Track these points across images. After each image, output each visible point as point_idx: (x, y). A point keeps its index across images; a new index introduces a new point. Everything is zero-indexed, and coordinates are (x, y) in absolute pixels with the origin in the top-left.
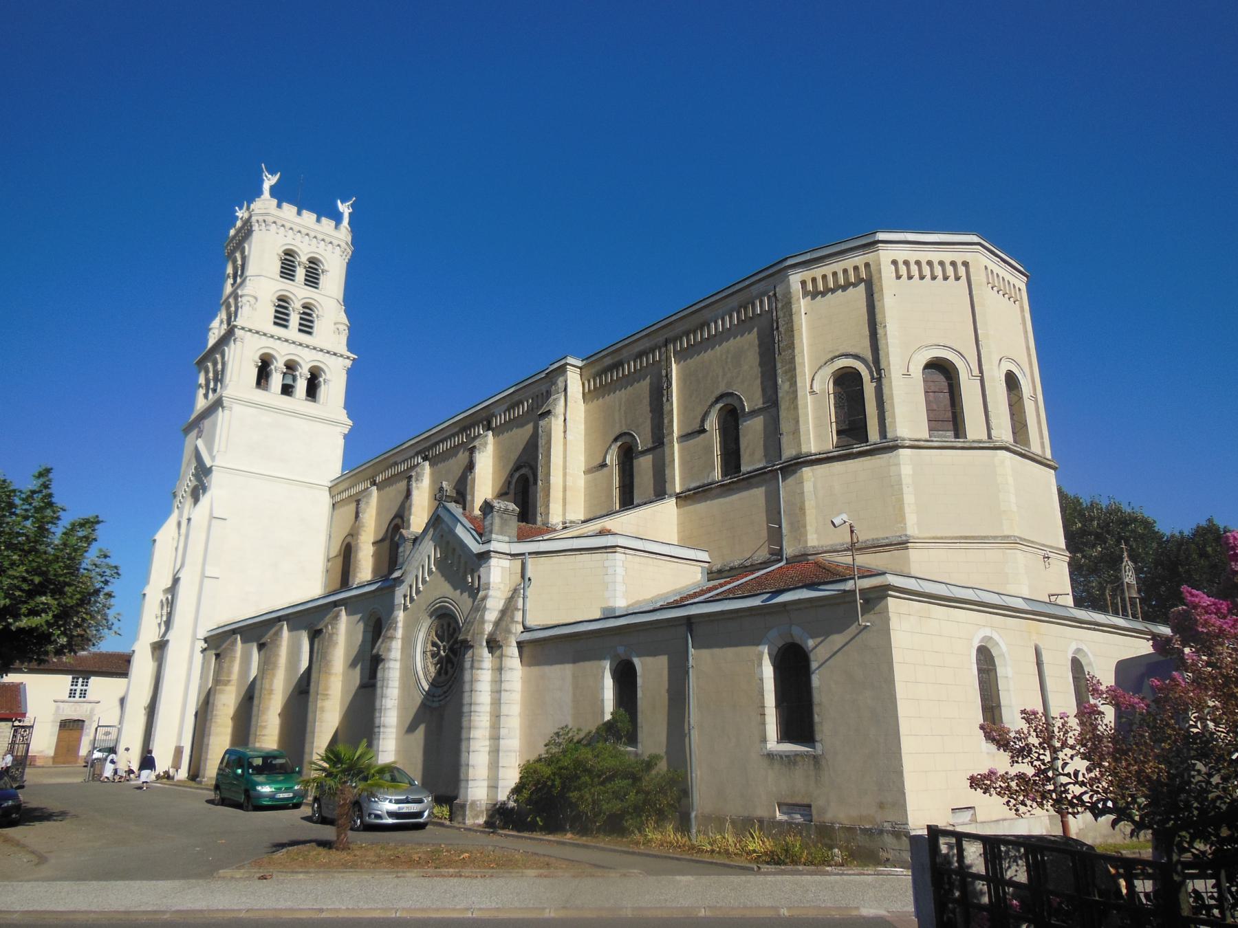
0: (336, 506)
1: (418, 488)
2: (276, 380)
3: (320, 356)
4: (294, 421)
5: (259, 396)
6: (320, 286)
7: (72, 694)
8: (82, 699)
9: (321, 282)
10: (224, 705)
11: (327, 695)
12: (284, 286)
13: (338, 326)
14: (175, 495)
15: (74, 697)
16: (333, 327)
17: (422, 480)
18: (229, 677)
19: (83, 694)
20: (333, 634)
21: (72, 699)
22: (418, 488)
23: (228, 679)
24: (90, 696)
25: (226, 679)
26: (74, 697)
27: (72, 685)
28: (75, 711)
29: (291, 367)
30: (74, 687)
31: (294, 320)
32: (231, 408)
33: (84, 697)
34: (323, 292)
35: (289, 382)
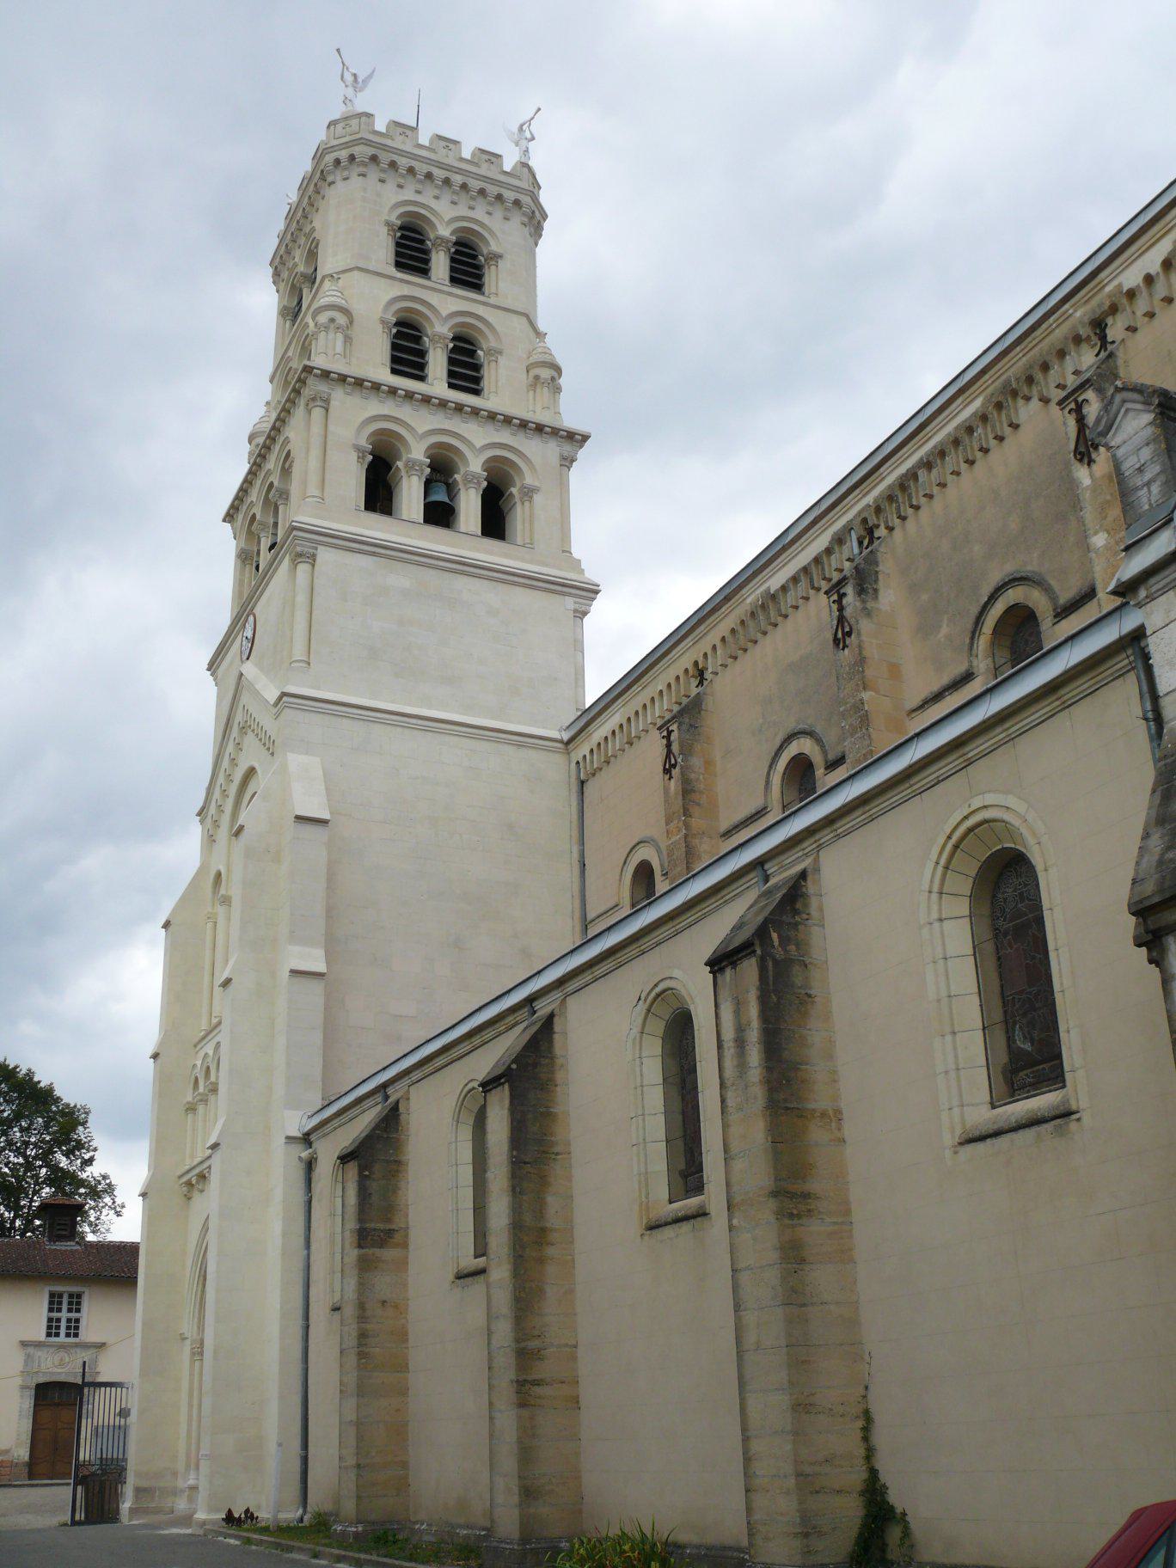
0: (588, 788)
1: (868, 613)
2: (411, 494)
3: (505, 436)
4: (464, 586)
5: (376, 527)
6: (486, 289)
7: (52, 1328)
8: (72, 1340)
9: (486, 279)
10: (384, 1302)
11: (806, 1196)
12: (407, 286)
13: (537, 371)
14: (280, 1445)
15: (57, 1335)
16: (523, 378)
17: (876, 591)
18: (389, 1221)
19: (74, 1328)
20: (789, 962)
21: (53, 1339)
22: (868, 613)
23: (388, 1227)
24: (88, 1333)
25: (381, 1226)
26: (57, 1335)
27: (77, 1321)
28: (61, 1364)
29: (440, 515)
30: (55, 1315)
31: (437, 363)
32: (314, 557)
33: (76, 1335)
34: (492, 300)
35: (440, 496)
